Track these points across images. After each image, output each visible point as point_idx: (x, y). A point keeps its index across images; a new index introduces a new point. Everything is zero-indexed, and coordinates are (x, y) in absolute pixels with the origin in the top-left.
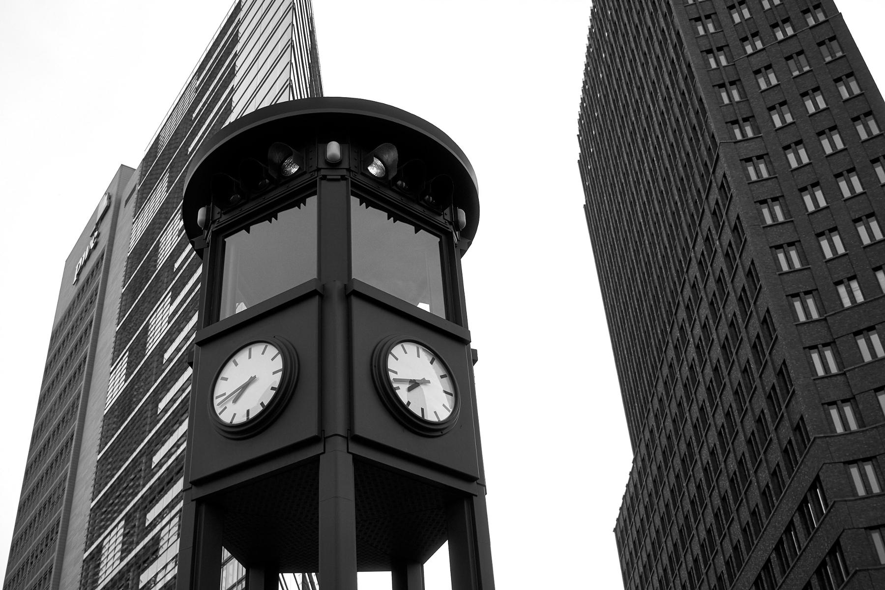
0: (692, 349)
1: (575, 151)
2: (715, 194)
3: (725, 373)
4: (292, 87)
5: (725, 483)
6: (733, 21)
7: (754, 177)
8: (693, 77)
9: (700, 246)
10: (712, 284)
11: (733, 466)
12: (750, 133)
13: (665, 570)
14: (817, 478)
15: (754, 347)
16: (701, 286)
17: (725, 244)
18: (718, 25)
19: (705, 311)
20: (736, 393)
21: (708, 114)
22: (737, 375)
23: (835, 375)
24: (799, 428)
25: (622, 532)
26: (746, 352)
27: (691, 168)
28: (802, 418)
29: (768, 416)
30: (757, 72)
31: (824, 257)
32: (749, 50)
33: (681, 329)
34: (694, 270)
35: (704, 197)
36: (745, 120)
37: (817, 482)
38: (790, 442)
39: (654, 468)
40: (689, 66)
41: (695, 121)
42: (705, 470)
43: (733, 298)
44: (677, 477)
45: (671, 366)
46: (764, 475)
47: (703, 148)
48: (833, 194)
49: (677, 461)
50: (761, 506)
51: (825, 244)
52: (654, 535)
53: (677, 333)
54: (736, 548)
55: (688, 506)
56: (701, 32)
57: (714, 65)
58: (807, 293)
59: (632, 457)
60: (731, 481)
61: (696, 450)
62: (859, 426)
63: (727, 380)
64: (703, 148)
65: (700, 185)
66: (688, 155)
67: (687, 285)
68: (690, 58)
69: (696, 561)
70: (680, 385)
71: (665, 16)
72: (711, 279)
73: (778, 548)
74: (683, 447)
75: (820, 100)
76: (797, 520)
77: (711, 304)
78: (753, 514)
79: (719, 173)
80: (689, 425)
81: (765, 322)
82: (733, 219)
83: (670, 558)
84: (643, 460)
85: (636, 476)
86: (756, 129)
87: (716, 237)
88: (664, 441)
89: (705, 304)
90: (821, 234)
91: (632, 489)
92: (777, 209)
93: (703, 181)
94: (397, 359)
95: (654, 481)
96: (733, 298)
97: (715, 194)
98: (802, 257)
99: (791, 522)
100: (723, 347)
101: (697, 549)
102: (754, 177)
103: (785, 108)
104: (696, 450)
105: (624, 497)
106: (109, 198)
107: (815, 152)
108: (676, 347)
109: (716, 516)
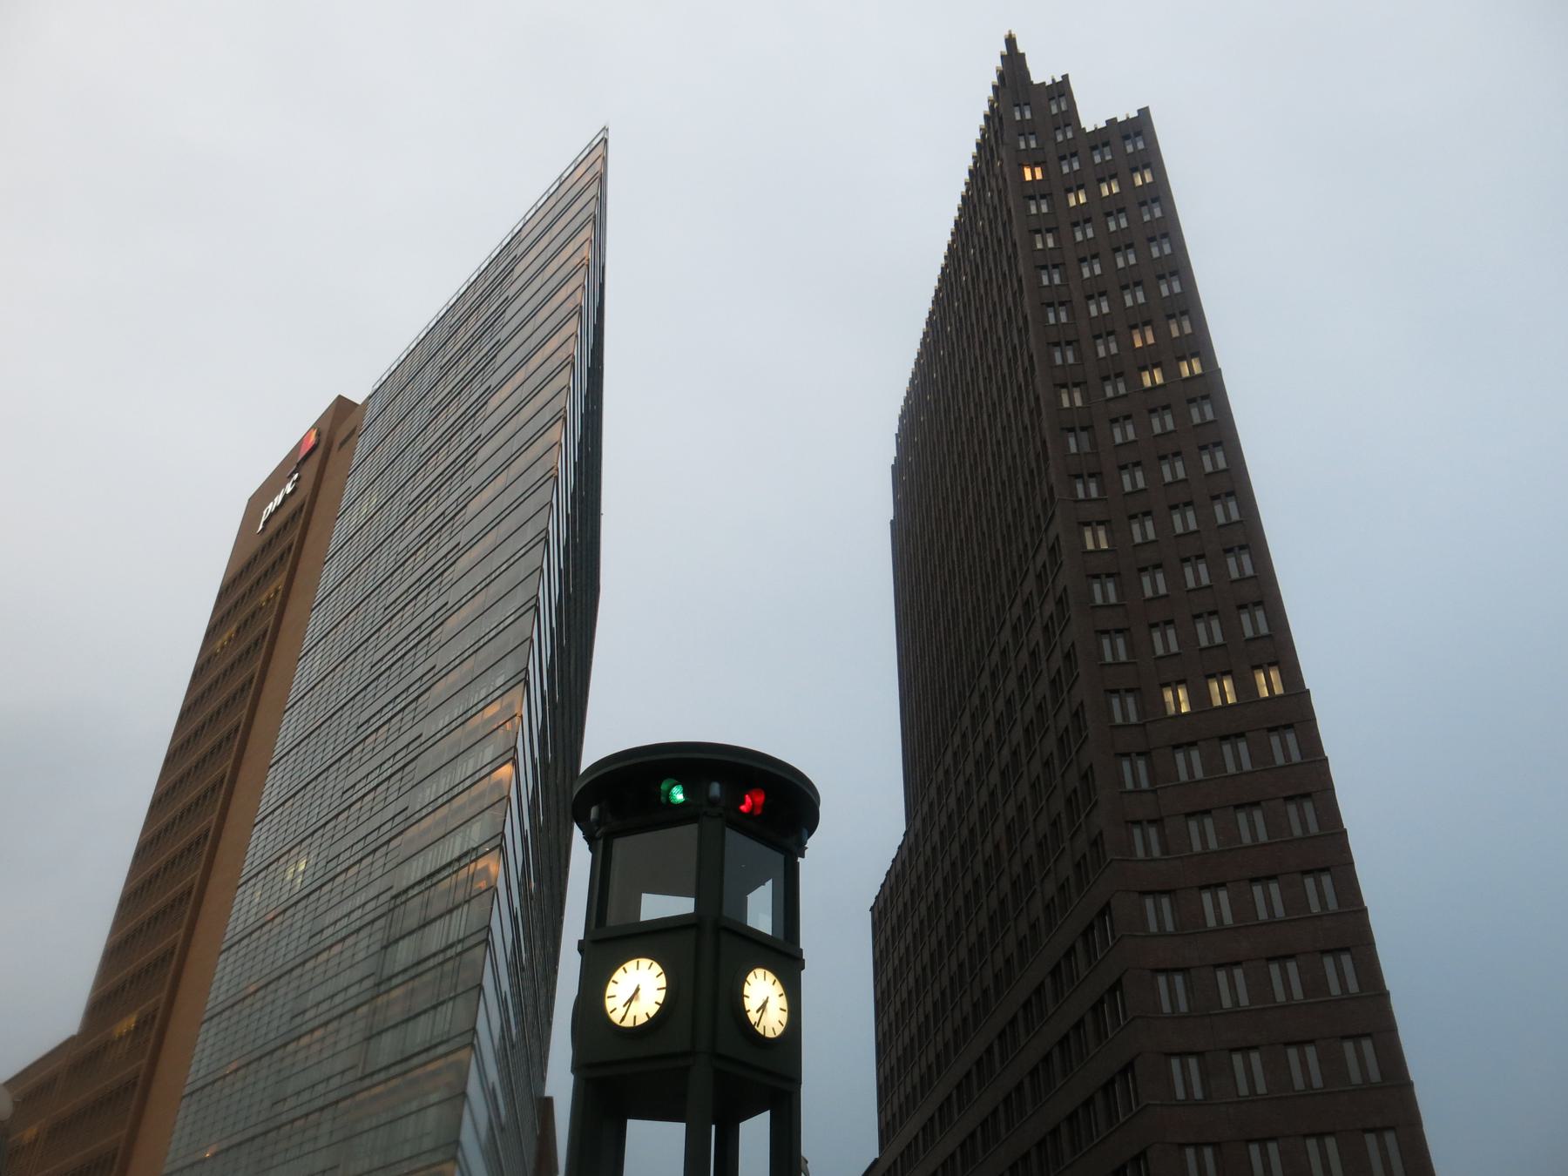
0: (990, 723)
1: (889, 453)
2: (1043, 555)
3: (1024, 761)
4: (538, 610)
5: (1005, 885)
6: (1097, 353)
7: (1081, 495)
8: (1039, 414)
9: (1017, 610)
10: (1024, 656)
11: (1017, 868)
12: (1094, 493)
13: (924, 969)
14: (1108, 904)
15: (1061, 740)
16: (1012, 655)
17: (1047, 614)
18: (1079, 355)
19: (1012, 683)
20: (1033, 786)
21: (1051, 462)
22: (1037, 766)
23: (1145, 791)
24: (1096, 843)
25: (882, 912)
26: (1051, 744)
27: (1022, 516)
28: (1101, 834)
29: (1064, 821)
30: (1114, 421)
31: (1154, 652)
32: (1110, 392)
33: (982, 696)
34: (1007, 634)
35: (1031, 554)
36: (1091, 475)
37: (1106, 910)
38: (1084, 856)
39: (928, 847)
40: (1037, 399)
41: (1034, 465)
42: (986, 864)
43: (1038, 626)
44: (953, 864)
45: (964, 736)
46: (1051, 888)
47: (1038, 498)
48: (1175, 580)
49: (956, 846)
50: (1042, 920)
51: (1157, 636)
52: (917, 925)
53: (976, 701)
54: (1008, 961)
55: (960, 902)
56: (1045, 281)
57: (1059, 361)
58: (1128, 691)
59: (904, 829)
60: (1014, 884)
61: (979, 839)
62: (1163, 853)
63: (1025, 769)
64: (1038, 498)
65: (1028, 539)
66: (1020, 500)
67: (996, 649)
68: (1016, 237)
69: (961, 966)
70: (971, 760)
71: (1019, 331)
72: (1025, 650)
73: (1055, 972)
74: (965, 832)
75: (1169, 419)
76: (1079, 946)
77: (1020, 678)
78: (1033, 927)
79: (1052, 534)
80: (975, 809)
81: (1077, 715)
82: (1059, 589)
83: (932, 955)
84: (916, 836)
85: (905, 852)
86: (1101, 488)
87: (1037, 604)
88: (944, 819)
89: (1013, 676)
90: (1155, 625)
91: (899, 867)
92: (1111, 587)
93: (1032, 536)
94: (638, 990)
95: (926, 864)
96: (1038, 626)
97: (1043, 555)
98: (1130, 648)
99: (1073, 948)
100: (1027, 731)
101: (963, 953)
102: (1081, 495)
103: (1111, 338)
104: (979, 839)
105: (888, 873)
106: (318, 434)
107: (1094, 195)
108: (973, 716)
109: (991, 919)
